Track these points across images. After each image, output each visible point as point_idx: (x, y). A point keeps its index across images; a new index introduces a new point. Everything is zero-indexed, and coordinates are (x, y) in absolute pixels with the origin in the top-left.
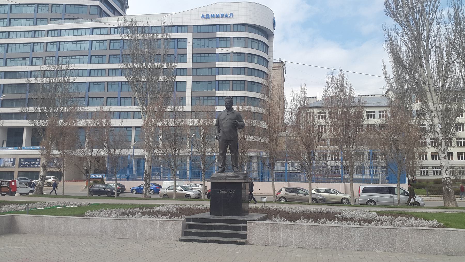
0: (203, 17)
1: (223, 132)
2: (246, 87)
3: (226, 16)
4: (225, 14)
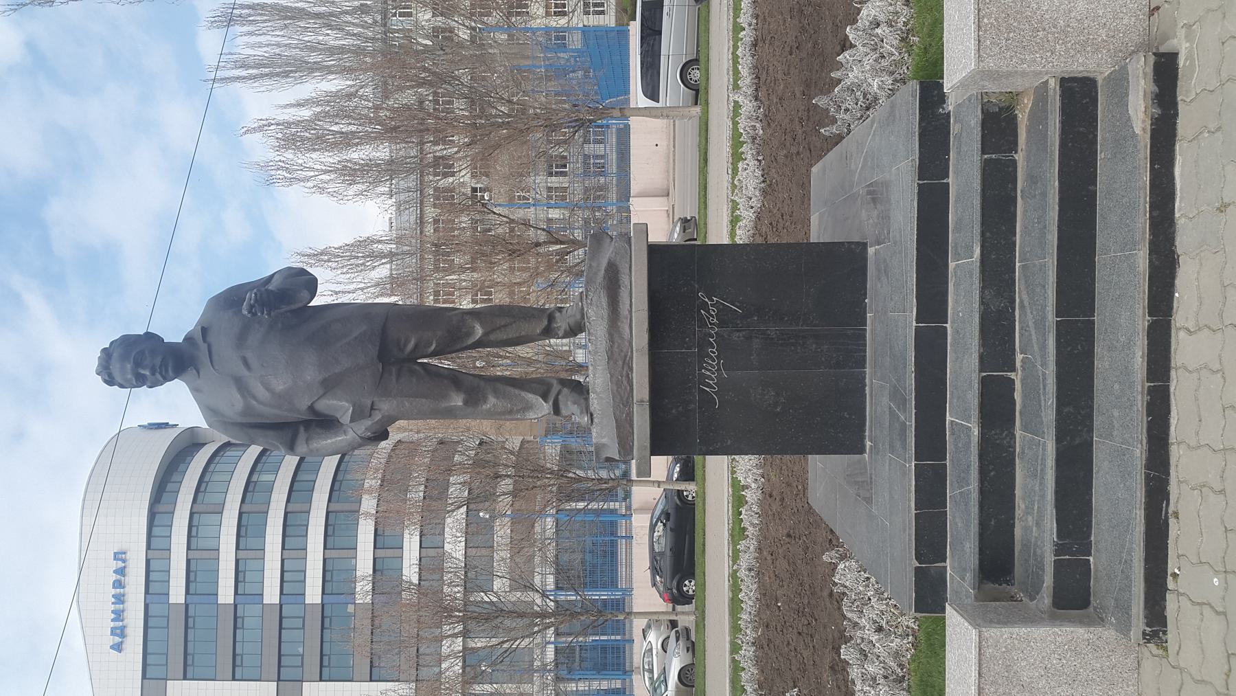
0: (118, 647)
1: (329, 385)
2: (346, 507)
3: (121, 572)
4: (114, 577)
